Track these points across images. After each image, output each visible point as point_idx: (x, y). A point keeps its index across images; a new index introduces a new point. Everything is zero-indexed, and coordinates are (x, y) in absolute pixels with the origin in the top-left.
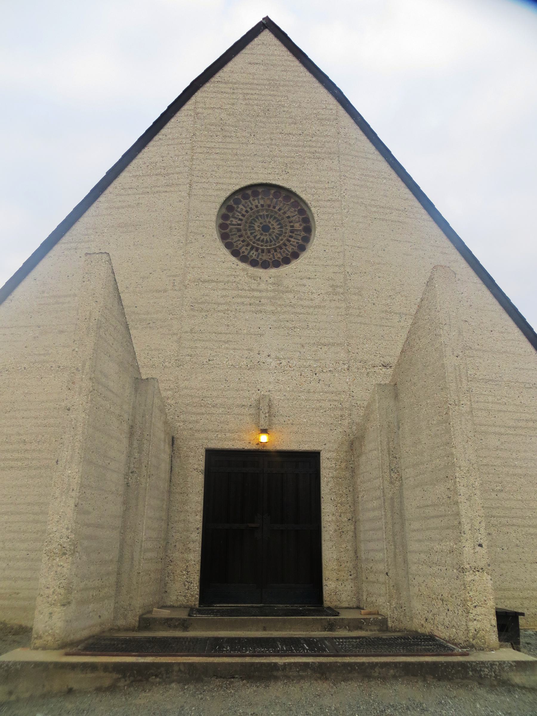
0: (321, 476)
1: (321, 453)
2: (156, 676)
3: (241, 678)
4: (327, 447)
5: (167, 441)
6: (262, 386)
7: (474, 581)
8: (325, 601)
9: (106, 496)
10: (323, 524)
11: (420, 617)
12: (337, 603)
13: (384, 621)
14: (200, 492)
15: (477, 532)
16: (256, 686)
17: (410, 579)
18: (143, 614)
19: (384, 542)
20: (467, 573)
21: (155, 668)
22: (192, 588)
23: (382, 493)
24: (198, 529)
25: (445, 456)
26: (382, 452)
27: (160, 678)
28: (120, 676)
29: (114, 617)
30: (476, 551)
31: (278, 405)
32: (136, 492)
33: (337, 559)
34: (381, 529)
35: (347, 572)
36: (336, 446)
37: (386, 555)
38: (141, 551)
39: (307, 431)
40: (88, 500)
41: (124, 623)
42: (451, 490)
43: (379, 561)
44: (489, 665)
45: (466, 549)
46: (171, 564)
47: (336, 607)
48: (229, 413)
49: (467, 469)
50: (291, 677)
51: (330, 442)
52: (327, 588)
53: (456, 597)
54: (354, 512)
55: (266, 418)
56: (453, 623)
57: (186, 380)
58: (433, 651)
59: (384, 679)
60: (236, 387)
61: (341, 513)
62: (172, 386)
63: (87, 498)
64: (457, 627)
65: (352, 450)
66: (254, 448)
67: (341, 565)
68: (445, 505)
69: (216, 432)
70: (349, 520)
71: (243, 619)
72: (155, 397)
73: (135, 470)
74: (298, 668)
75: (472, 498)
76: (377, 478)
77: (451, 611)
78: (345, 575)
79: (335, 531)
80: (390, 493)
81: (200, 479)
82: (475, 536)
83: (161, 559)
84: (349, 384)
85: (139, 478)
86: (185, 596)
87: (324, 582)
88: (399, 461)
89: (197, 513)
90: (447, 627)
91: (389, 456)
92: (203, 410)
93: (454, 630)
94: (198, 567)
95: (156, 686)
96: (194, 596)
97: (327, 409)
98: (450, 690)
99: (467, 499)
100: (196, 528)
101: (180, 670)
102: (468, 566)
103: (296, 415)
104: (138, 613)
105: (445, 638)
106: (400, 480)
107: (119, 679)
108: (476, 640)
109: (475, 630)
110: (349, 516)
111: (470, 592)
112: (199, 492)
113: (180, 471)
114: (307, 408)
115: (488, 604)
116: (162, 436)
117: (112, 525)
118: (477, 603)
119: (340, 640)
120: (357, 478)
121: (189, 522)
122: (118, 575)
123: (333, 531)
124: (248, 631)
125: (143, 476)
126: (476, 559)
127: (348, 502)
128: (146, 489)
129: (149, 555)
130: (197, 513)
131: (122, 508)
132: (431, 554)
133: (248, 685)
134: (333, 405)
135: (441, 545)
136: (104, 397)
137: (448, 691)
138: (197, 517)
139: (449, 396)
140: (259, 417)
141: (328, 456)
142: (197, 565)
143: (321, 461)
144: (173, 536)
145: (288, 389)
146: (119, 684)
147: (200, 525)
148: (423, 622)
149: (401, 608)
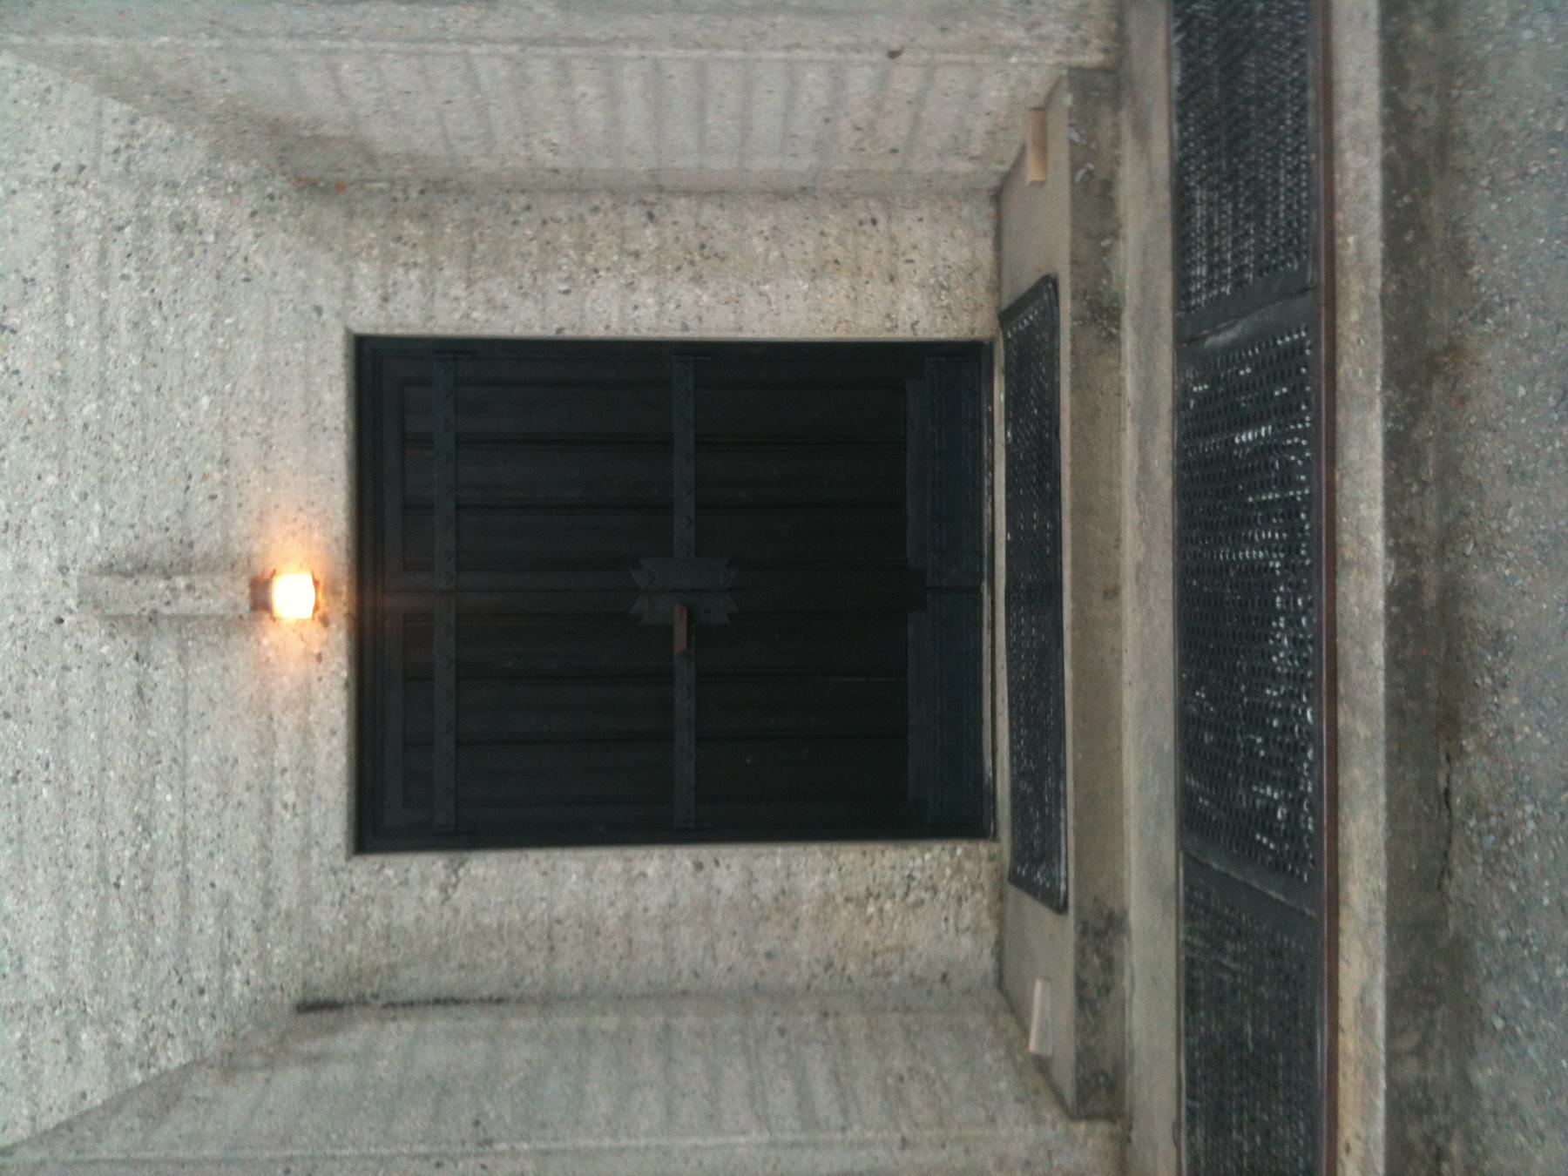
2: (1440, 1155)
3: (1448, 759)
4: (330, 303)
5: (315, 1046)
6: (36, 604)
10: (670, 330)
12: (981, 281)
13: (1082, 81)
14: (545, 865)
18: (1059, 1099)
22: (928, 872)
23: (541, 51)
24: (699, 866)
27: (1448, 1138)
31: (132, 526)
33: (813, 279)
36: (325, 261)
37: (818, 55)
38: (815, 1146)
47: (996, 288)
48: (180, 760)
50: (1446, 519)
51: (305, 288)
54: (619, 191)
55: (198, 585)
57: (20, 968)
60: (49, 730)
61: (623, 252)
62: (54, 1031)
65: (340, 187)
67: (836, 262)
69: (270, 812)
70: (651, 216)
71: (1077, 689)
72: (93, 1156)
76: (470, 68)
78: (872, 247)
79: (697, 280)
83: (826, 1015)
84: (15, 185)
86: (960, 900)
87: (903, 334)
89: (635, 873)
92: (166, 879)
94: (850, 855)
95: (1486, 1155)
96: (959, 863)
97: (146, 294)
100: (694, 876)
101: (1419, 1052)
103: (178, 443)
104: (1060, 1127)
110: (634, 215)
112: (545, 873)
113: (453, 964)
114: (142, 394)
116: (293, 1077)
120: (471, 169)
123: (698, 291)
124: (1119, 662)
128: (546, 1153)
129: (823, 1095)
133: (1489, 728)
134: (125, 265)
138: (650, 871)
140: (195, 618)
141: (373, 299)
142: (841, 859)
143: (398, 331)
144: (730, 969)
145: (51, 480)
147: (683, 857)
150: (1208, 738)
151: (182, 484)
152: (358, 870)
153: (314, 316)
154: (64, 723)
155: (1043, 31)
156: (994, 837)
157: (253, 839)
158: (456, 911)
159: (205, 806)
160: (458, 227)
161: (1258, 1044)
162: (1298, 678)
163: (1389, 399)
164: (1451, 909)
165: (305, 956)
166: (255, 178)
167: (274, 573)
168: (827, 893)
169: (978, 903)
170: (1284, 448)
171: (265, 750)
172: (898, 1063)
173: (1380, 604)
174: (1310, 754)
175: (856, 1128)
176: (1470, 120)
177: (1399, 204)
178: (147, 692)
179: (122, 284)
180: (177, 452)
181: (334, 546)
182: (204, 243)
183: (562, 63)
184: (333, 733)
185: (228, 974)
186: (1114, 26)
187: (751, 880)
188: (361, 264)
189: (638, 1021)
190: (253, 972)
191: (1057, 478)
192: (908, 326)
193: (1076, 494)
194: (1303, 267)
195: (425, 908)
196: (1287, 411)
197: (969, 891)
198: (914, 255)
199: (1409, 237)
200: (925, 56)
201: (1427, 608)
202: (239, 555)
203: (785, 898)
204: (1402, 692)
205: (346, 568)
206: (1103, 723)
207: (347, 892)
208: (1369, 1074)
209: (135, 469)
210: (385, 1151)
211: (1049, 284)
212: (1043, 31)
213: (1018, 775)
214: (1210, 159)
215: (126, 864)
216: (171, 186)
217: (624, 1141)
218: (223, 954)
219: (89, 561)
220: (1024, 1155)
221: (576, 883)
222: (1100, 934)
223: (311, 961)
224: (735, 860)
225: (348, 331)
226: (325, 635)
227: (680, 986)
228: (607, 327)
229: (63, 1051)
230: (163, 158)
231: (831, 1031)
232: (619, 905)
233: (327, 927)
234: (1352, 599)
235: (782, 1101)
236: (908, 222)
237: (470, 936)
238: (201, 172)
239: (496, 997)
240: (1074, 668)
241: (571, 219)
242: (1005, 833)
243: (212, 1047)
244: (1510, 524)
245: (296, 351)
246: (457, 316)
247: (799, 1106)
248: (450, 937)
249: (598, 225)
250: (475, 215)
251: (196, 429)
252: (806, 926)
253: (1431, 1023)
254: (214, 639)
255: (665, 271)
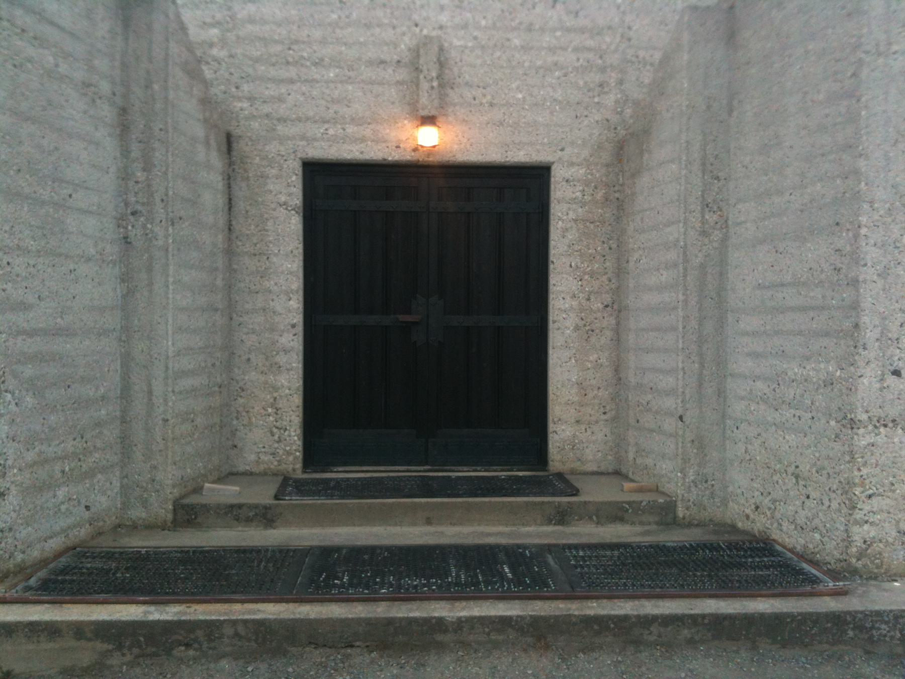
0: (552, 217)
1: (553, 168)
2: (188, 646)
3: (367, 646)
5: (213, 142)
6: (424, 14)
7: (873, 446)
8: (552, 461)
9: (72, 268)
10: (553, 315)
11: (743, 501)
12: (577, 465)
14: (296, 252)
15: (892, 345)
16: (398, 664)
17: (727, 428)
18: (182, 497)
19: (678, 355)
20: (861, 431)
21: (182, 632)
23: (681, 255)
24: (293, 326)
25: (838, 176)
26: (689, 166)
27: (196, 650)
28: (111, 647)
29: (123, 503)
30: (885, 385)
31: (461, 61)
32: (146, 255)
34: (674, 329)
35: (597, 408)
36: (585, 153)
37: (681, 383)
38: (166, 378)
39: (523, 120)
40: (19, 279)
41: (144, 515)
42: (844, 253)
43: (665, 392)
44: (892, 618)
45: (865, 381)
46: (242, 394)
47: (573, 472)
48: (350, 81)
49: (887, 206)
50: (473, 644)
52: (556, 437)
53: (828, 474)
54: (618, 292)
56: (817, 521)
58: (773, 584)
59: (669, 647)
61: (590, 293)
62: (219, 16)
63: (18, 276)
64: (825, 532)
65: (620, 161)
66: (409, 158)
67: (586, 395)
68: (826, 285)
69: (324, 122)
70: (607, 306)
71: (384, 504)
73: (139, 207)
74: (488, 627)
75: (890, 271)
77: (814, 499)
78: (592, 412)
79: (577, 328)
80: (700, 255)
81: (295, 224)
82: (889, 353)
83: (220, 387)
84: (622, 9)
85: (149, 226)
86: (274, 454)
87: (551, 427)
88: (724, 185)
89: (291, 295)
90: (801, 527)
91: (703, 177)
92: (292, 72)
93: (816, 535)
94: (297, 400)
95: (188, 666)
96: (291, 454)
98: (806, 669)
99: (879, 275)
100: (289, 324)
101: (237, 634)
102: (864, 417)
104: (170, 496)
105: (795, 548)
106: (723, 227)
107: (110, 651)
108: (864, 560)
109: (865, 542)
110: (607, 298)
111: (862, 468)
112: (292, 252)
114: (523, 66)
115: (898, 491)
116: (199, 131)
117: (97, 326)
118: (875, 489)
119: (578, 552)
120: (628, 222)
121: (274, 312)
122: (124, 424)
124: (396, 525)
125: (159, 221)
126: (884, 402)
127: (606, 271)
128: (167, 250)
129: (187, 383)
130: (291, 295)
131: (118, 290)
132: (781, 383)
133: (382, 662)
135: (804, 368)
136: (35, 38)
137: (802, 670)
138: (291, 302)
139: (865, 31)
140: (418, 90)
141: (567, 175)
142: (295, 395)
143: (552, 187)
144: (242, 340)
145: (483, 23)
146: (109, 662)
147: (298, 319)
148: (748, 511)
149: (706, 482)
150: (366, 557)
151: (481, 84)
152: (295, 163)
153: (560, 148)
154: (368, 26)
155: (693, 489)
156: (304, 472)
157: (311, 114)
158: (274, 210)
159: (327, 92)
160: (601, 216)
161: (228, 575)
162: (400, 587)
163: (526, 618)
164: (300, 649)
165: (254, 137)
166: (624, 121)
167: (439, 127)
168: (279, 388)
169: (272, 463)
170: (503, 582)
171: (353, 120)
172: (199, 420)
173: (436, 615)
174: (366, 591)
175: (174, 398)
176: (647, 654)
177: (610, 622)
178: (382, 66)
179: (575, 58)
180: (496, 83)
181: (451, 155)
182: (594, 97)
183: (675, 265)
184: (362, 153)
185: (246, 101)
186: (696, 522)
187: (286, 351)
188: (584, 170)
189: (220, 296)
190: (246, 112)
191: (484, 496)
192: (555, 429)
193: (476, 504)
194: (582, 587)
195: (276, 195)
196: (519, 582)
197: (278, 459)
198: (589, 433)
199: (596, 627)
200: (681, 433)
201: (434, 636)
202: (447, 110)
203: (277, 368)
204: (398, 625)
205: (440, 160)
206: (367, 517)
207: (285, 158)
208: (225, 614)
209: (488, 62)
210: (170, 175)
211: (575, 492)
212: (693, 489)
213: (338, 482)
214: (632, 557)
215: (300, 54)
216: (621, 82)
217: (171, 287)
218: (255, 99)
219: (445, 40)
220: (157, 478)
221: (287, 267)
222: (264, 516)
223: (251, 140)
224: (296, 343)
225: (553, 163)
226: (409, 150)
227: (235, 316)
228: (554, 285)
229: (208, 20)
230: (634, 79)
231: (213, 389)
232: (276, 288)
233: (267, 148)
234: (437, 606)
235: (186, 363)
236: (604, 429)
237: (262, 216)
238: (627, 96)
239: (232, 228)
240: (393, 503)
241: (606, 268)
242: (306, 476)
243: (214, 90)
244: (472, 668)
245: (543, 139)
246: (559, 214)
247: (183, 371)
248: (262, 206)
249: (602, 281)
250: (607, 224)
251: (507, 91)
252: (262, 378)
253: (249, 640)
254: (408, 98)
255: (581, 313)
